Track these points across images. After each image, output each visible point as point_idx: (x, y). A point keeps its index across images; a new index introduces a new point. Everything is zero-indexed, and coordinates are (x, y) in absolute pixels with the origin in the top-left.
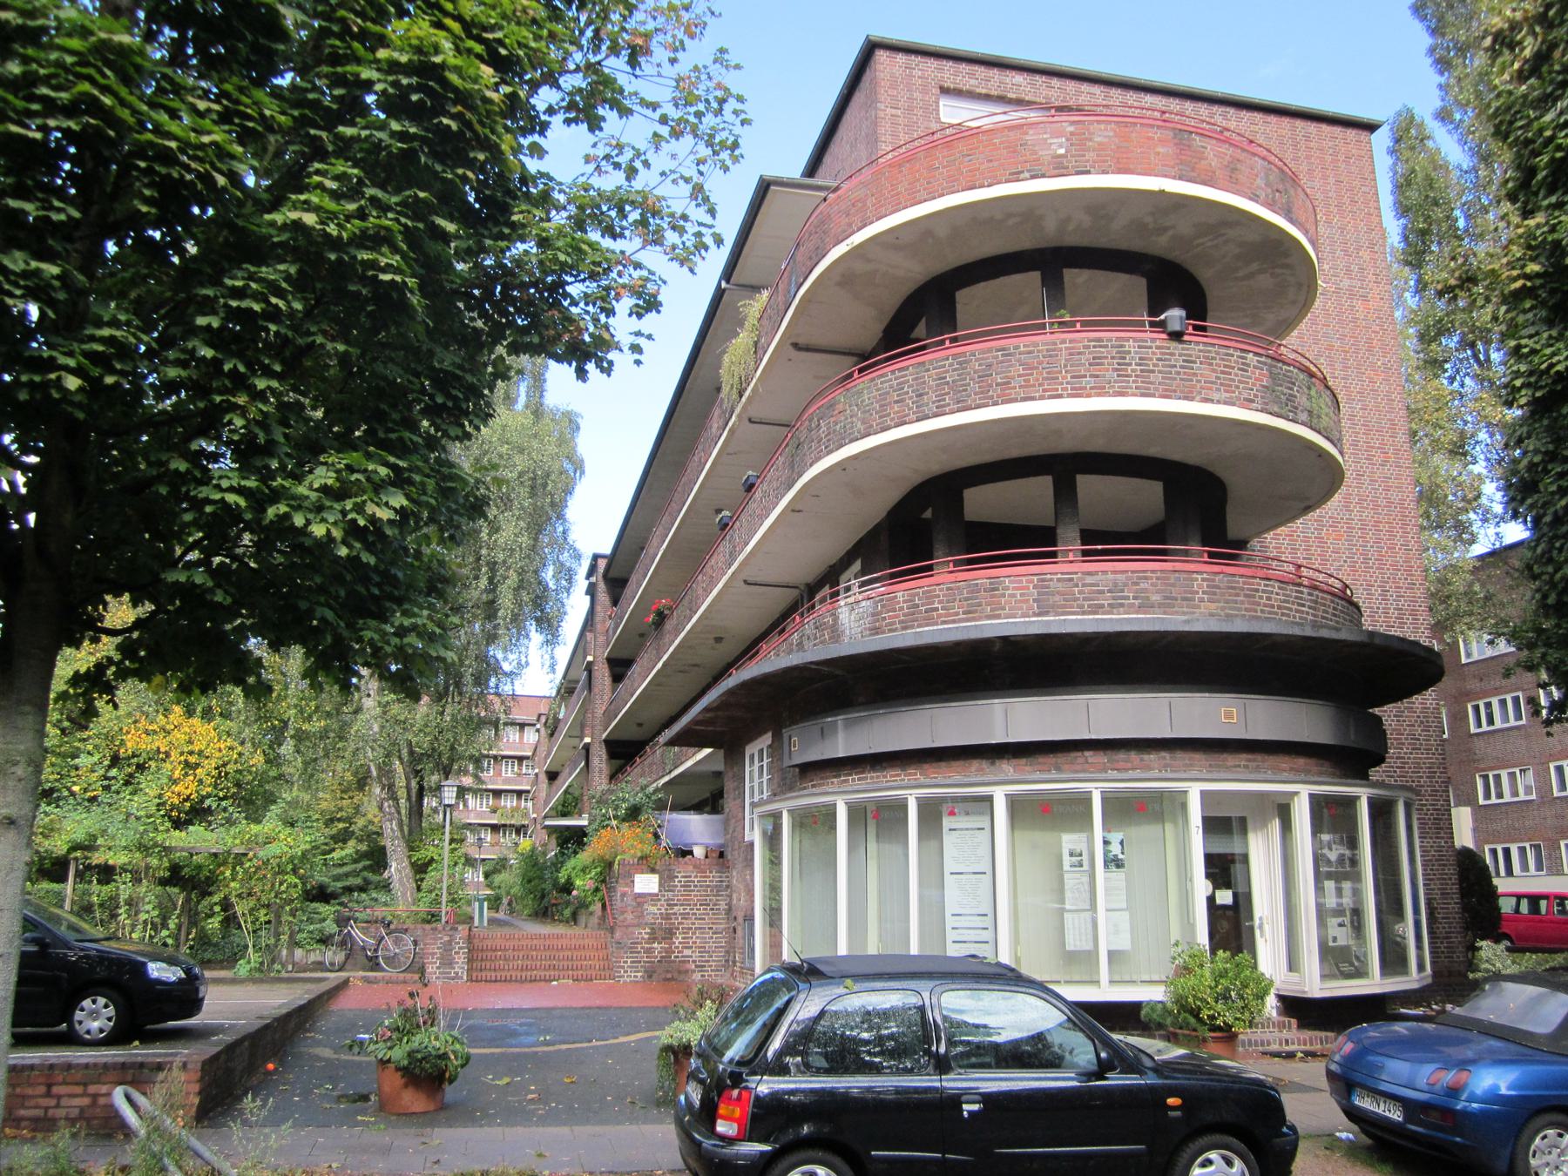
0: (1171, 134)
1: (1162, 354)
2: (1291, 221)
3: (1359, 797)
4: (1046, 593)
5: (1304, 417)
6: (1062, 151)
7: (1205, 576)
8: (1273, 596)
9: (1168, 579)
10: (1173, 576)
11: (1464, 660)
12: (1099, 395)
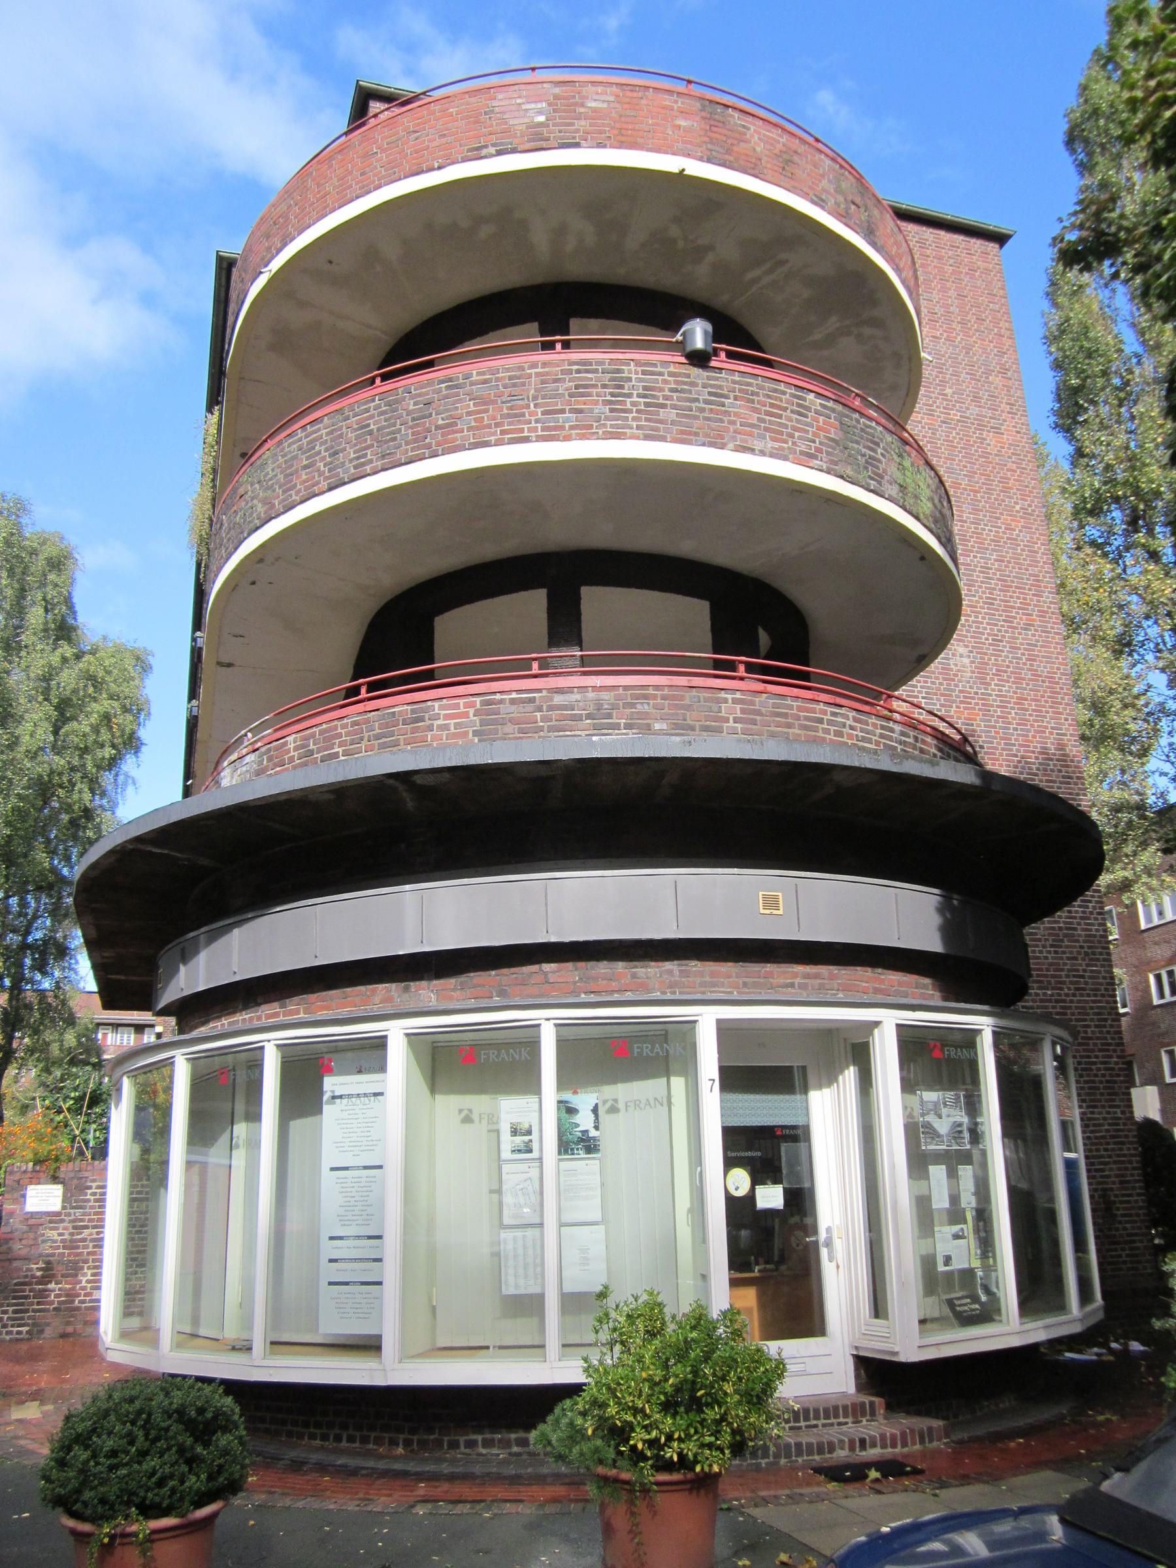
0: (698, 105)
1: (676, 382)
2: (873, 245)
3: (979, 1031)
4: (495, 722)
5: (893, 491)
6: (542, 119)
7: (738, 695)
8: (846, 730)
9: (682, 698)
10: (690, 696)
11: (1143, 926)
12: (582, 437)
